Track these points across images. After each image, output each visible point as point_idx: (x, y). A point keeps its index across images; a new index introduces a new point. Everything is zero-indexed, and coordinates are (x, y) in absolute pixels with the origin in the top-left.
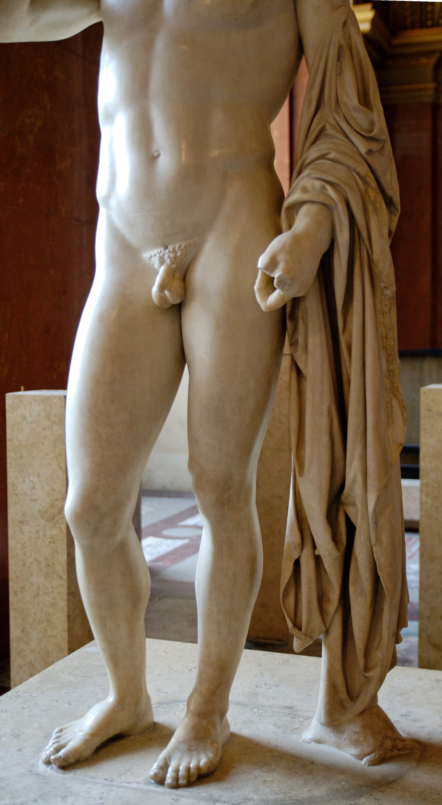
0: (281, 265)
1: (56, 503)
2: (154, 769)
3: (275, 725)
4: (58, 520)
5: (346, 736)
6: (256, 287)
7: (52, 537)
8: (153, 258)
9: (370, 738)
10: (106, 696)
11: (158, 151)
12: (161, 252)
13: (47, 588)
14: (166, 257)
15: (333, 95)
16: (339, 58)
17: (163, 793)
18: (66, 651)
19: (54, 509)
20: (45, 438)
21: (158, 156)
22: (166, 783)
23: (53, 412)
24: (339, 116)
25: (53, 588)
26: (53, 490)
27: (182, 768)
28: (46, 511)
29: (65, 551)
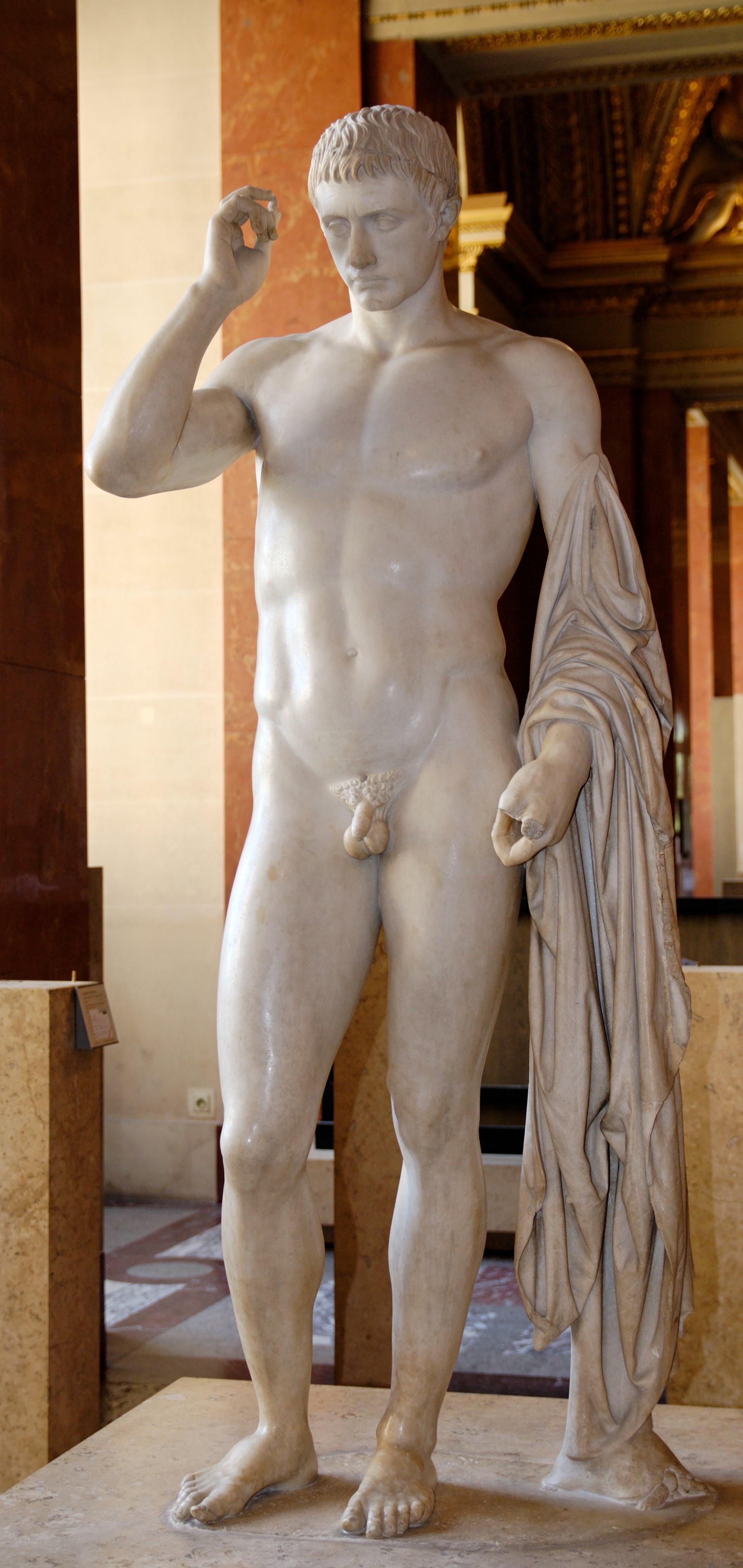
0: (532, 807)
1: (30, 1182)
2: (346, 1516)
3: (497, 1473)
4: (33, 1212)
5: (610, 1472)
6: (493, 834)
7: (21, 1244)
8: (345, 791)
9: (646, 1474)
11: (354, 649)
12: (357, 783)
13: (10, 1339)
14: (364, 791)
15: (586, 573)
17: (366, 1544)
18: (44, 1454)
19: (25, 1194)
20: (11, 1065)
21: (355, 655)
22: (367, 1532)
23: (28, 1019)
24: (593, 601)
25: (20, 1337)
26: (25, 1158)
27: (388, 1510)
28: (11, 1197)
29: (46, 1269)
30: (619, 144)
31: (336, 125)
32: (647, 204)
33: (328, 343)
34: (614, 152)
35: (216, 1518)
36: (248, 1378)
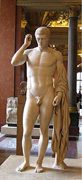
6: (53, 103)
10: (24, 162)
16: (62, 71)
27: (39, 170)
30: (39, 16)
31: (38, 28)
32: (41, 22)
33: (35, 50)
34: (38, 16)
35: (22, 171)
36: (23, 155)
